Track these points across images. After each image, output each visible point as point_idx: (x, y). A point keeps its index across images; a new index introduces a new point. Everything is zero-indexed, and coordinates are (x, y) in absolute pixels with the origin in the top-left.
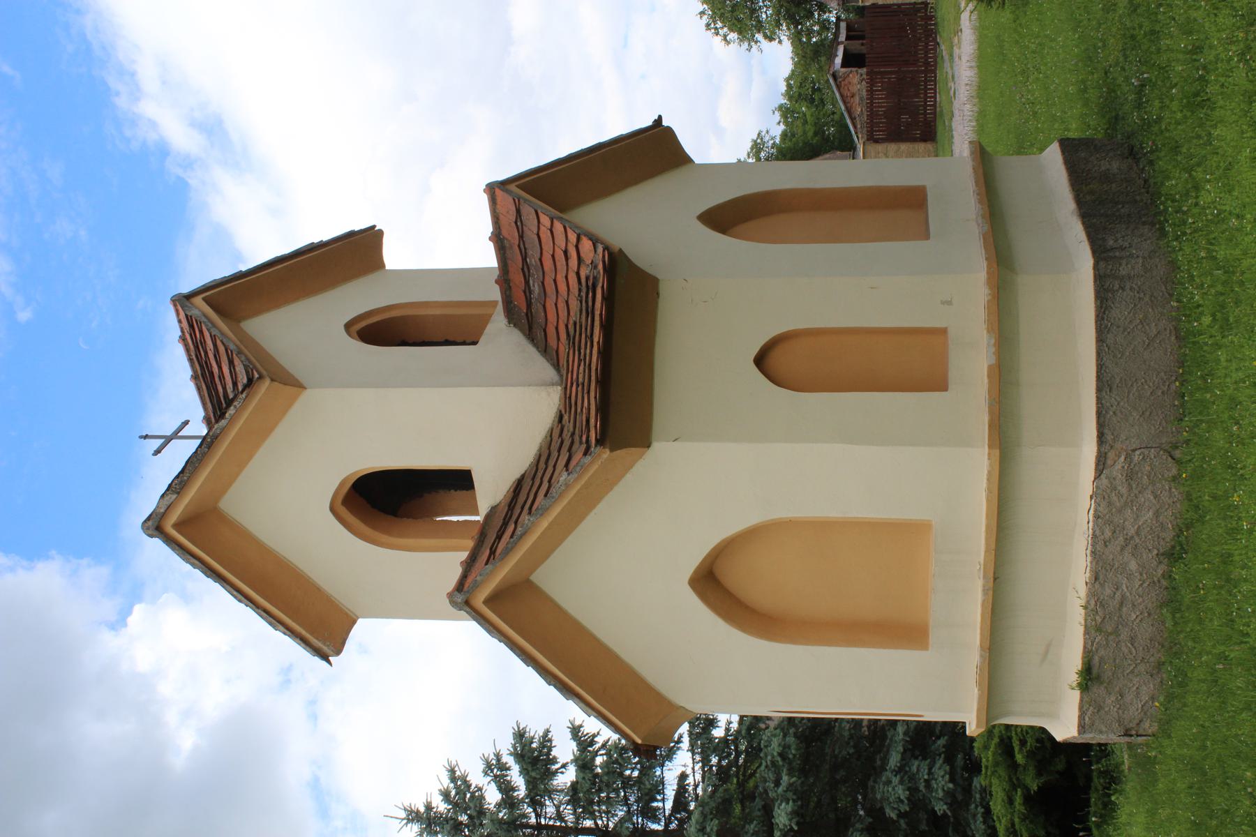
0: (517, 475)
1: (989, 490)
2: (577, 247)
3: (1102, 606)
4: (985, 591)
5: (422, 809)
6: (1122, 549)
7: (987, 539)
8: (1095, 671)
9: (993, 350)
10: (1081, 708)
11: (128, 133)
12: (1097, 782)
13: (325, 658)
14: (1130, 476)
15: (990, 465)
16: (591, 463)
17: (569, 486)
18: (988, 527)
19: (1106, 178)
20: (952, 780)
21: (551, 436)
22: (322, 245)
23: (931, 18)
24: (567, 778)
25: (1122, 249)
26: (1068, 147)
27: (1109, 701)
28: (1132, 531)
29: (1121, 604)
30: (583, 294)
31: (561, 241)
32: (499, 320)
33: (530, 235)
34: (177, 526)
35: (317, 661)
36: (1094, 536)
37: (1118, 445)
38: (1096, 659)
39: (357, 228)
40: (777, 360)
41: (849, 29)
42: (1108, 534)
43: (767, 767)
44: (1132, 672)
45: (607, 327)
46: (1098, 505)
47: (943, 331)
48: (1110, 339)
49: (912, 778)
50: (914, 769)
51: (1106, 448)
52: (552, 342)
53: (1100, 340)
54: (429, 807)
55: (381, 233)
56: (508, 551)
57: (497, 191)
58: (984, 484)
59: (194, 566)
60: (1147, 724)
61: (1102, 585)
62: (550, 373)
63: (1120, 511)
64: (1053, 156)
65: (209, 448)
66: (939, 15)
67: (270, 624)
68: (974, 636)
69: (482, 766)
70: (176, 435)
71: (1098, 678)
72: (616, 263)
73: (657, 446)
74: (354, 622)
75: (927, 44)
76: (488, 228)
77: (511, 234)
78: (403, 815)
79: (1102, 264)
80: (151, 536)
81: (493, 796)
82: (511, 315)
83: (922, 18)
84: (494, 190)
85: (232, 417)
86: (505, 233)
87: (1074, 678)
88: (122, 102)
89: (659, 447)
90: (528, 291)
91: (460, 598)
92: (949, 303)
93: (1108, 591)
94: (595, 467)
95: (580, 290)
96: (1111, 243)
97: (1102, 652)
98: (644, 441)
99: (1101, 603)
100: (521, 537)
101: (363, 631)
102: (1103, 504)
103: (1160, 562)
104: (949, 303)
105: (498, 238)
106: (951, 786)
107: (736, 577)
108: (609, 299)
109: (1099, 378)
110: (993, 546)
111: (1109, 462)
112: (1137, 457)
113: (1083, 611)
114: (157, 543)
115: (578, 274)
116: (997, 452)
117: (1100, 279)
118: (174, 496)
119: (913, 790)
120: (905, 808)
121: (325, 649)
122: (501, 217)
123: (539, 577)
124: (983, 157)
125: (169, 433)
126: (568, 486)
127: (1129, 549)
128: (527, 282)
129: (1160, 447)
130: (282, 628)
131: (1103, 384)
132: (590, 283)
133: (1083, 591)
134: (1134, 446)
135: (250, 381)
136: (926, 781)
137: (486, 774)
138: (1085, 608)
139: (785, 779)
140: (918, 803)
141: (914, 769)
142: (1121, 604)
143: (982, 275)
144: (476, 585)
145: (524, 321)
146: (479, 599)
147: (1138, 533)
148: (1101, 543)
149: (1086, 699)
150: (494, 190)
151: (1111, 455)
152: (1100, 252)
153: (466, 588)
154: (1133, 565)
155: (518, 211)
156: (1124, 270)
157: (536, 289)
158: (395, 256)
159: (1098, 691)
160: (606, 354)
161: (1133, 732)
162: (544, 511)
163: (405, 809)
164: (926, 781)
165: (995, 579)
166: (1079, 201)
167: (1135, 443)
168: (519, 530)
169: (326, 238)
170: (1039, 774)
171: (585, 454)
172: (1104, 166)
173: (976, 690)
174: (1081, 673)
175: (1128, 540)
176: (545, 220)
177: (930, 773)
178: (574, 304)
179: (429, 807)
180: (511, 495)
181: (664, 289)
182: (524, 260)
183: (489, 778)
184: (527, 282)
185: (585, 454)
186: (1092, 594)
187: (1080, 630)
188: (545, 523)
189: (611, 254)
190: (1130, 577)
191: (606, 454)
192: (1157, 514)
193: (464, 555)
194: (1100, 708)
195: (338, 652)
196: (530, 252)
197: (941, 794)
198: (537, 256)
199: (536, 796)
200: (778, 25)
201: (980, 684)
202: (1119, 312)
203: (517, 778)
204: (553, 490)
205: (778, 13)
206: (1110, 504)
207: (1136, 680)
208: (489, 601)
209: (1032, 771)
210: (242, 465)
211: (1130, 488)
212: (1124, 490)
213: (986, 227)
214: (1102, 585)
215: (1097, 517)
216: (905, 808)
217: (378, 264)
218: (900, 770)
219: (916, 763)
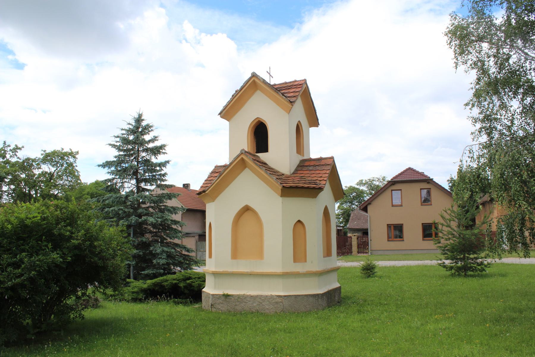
0: (267, 163)
1: (272, 272)
2: (323, 180)
3: (245, 298)
4: (247, 272)
5: (142, 118)
6: (259, 302)
7: (259, 272)
8: (228, 297)
9: (303, 272)
10: (218, 294)
11: (306, 13)
12: (184, 300)
13: (220, 114)
14: (277, 303)
15: (278, 273)
16: (278, 184)
17: (272, 179)
18: (263, 272)
19: (335, 297)
20: (162, 264)
21: (272, 169)
22: (316, 113)
23: (348, 254)
24: (154, 160)
25: (323, 300)
26: (339, 288)
27: (220, 301)
28: (263, 304)
29: (245, 302)
30: (312, 181)
31: (324, 176)
32: (301, 158)
33: (324, 168)
34: (254, 81)
35: (219, 112)
36: (262, 296)
37: (284, 300)
38: (231, 297)
39: (319, 121)
40: (299, 225)
41: (341, 230)
42: (263, 299)
43: (161, 215)
44: (228, 305)
45: (308, 188)
46: (270, 296)
47: (306, 261)
48: (305, 297)
49: (161, 254)
50: (164, 254)
51: (283, 297)
52: (299, 172)
53: (306, 295)
54: (143, 120)
55: (318, 127)
56: (256, 164)
57: (332, 160)
58: (225, 270)
59: (244, 84)
60: (214, 309)
61: (250, 298)
62: (292, 172)
63: (268, 301)
64: (337, 285)
65: (275, 91)
66: (349, 256)
67: (229, 101)
68: (230, 270)
69: (156, 135)
70: (270, 75)
71: (226, 298)
72: (321, 189)
73: (281, 199)
74: (228, 121)
75: (340, 253)
76: (323, 156)
77: (323, 162)
78: (140, 113)
79: (320, 295)
80: (252, 74)
81: (147, 138)
82: (303, 161)
83: (348, 251)
84: (332, 158)
85: (283, 97)
86: (323, 161)
87: (226, 292)
88: (315, 11)
89: (281, 199)
90: (310, 166)
91: (243, 152)
92: (312, 263)
93: (248, 299)
94: (277, 185)
95: (313, 180)
96: (324, 297)
97: (233, 299)
98: (282, 196)
99: (245, 298)
100: (259, 167)
101: (225, 123)
102: (270, 297)
103: (256, 310)
104: (312, 263)
105: (320, 159)
106: (161, 264)
107: (247, 215)
108: (314, 188)
109: (297, 295)
110: (258, 274)
111: (280, 298)
112: (281, 304)
113: (243, 294)
114: (250, 75)
115: (317, 180)
116: (282, 274)
117: (318, 295)
118: (262, 81)
119: (158, 254)
120: (154, 252)
121: (222, 114)
122: (326, 160)
123: (247, 169)
124: (335, 270)
125: (271, 74)
126: (273, 179)
127: (259, 303)
128: (312, 166)
129: (283, 309)
130: (228, 104)
131: (296, 296)
132: (316, 183)
133: (248, 294)
134: (284, 303)
135: (291, 102)
136: (161, 257)
137: (154, 136)
138: (244, 294)
139: (160, 220)
140: (155, 256)
141: (164, 254)
142: (245, 302)
143: (318, 270)
144: (247, 156)
145: (302, 165)
146: (243, 156)
147: (263, 305)
148: (260, 297)
149: (221, 296)
150: (332, 158)
151: (281, 298)
152: (323, 295)
153: (246, 153)
154: (255, 304)
155: (329, 165)
156: (320, 300)
157: (311, 168)
158: (312, 130)
159: (223, 298)
160: (302, 188)
161: (212, 306)
162: (266, 173)
163: (142, 113)
164: (161, 257)
165: (250, 274)
166: (331, 291)
167: (284, 303)
168: (261, 167)
169: (317, 114)
170: (184, 286)
171: (281, 183)
172: (337, 296)
173: (221, 271)
174: (227, 294)
175: (261, 303)
176: (328, 172)
177: (164, 258)
178: (310, 179)
179: (143, 120)
180: (264, 162)
181: (314, 199)
182: (317, 165)
183: (152, 137)
184: (312, 166)
185: (281, 183)
186: (248, 296)
187: (238, 293)
188: (263, 173)
189: (323, 188)
190: (252, 304)
191: (280, 188)
192: (268, 309)
193: (246, 150)
194: (218, 299)
195: (221, 117)
196: (319, 167)
197: (159, 261)
198: (319, 169)
199: (147, 150)
200: (342, 209)
201: (223, 272)
202: (311, 299)
203: (151, 145)
204: (271, 175)
205: (345, 210)
206: (270, 299)
207: (226, 306)
208: (242, 159)
209: (184, 285)
210: (269, 97)
211: (274, 303)
212: (273, 301)
213: (326, 270)
214: (250, 298)
215: (267, 296)
216: (154, 252)
217: (311, 126)
218: (163, 251)
219: (165, 255)
